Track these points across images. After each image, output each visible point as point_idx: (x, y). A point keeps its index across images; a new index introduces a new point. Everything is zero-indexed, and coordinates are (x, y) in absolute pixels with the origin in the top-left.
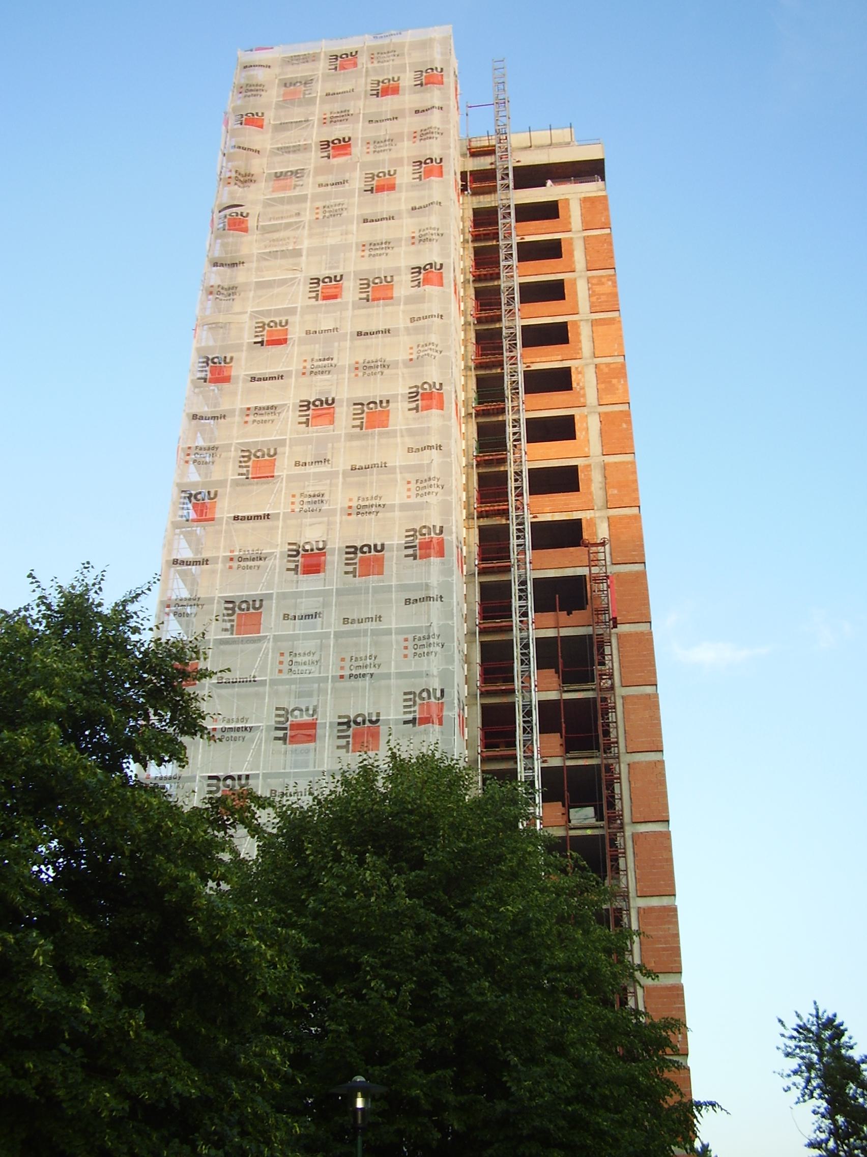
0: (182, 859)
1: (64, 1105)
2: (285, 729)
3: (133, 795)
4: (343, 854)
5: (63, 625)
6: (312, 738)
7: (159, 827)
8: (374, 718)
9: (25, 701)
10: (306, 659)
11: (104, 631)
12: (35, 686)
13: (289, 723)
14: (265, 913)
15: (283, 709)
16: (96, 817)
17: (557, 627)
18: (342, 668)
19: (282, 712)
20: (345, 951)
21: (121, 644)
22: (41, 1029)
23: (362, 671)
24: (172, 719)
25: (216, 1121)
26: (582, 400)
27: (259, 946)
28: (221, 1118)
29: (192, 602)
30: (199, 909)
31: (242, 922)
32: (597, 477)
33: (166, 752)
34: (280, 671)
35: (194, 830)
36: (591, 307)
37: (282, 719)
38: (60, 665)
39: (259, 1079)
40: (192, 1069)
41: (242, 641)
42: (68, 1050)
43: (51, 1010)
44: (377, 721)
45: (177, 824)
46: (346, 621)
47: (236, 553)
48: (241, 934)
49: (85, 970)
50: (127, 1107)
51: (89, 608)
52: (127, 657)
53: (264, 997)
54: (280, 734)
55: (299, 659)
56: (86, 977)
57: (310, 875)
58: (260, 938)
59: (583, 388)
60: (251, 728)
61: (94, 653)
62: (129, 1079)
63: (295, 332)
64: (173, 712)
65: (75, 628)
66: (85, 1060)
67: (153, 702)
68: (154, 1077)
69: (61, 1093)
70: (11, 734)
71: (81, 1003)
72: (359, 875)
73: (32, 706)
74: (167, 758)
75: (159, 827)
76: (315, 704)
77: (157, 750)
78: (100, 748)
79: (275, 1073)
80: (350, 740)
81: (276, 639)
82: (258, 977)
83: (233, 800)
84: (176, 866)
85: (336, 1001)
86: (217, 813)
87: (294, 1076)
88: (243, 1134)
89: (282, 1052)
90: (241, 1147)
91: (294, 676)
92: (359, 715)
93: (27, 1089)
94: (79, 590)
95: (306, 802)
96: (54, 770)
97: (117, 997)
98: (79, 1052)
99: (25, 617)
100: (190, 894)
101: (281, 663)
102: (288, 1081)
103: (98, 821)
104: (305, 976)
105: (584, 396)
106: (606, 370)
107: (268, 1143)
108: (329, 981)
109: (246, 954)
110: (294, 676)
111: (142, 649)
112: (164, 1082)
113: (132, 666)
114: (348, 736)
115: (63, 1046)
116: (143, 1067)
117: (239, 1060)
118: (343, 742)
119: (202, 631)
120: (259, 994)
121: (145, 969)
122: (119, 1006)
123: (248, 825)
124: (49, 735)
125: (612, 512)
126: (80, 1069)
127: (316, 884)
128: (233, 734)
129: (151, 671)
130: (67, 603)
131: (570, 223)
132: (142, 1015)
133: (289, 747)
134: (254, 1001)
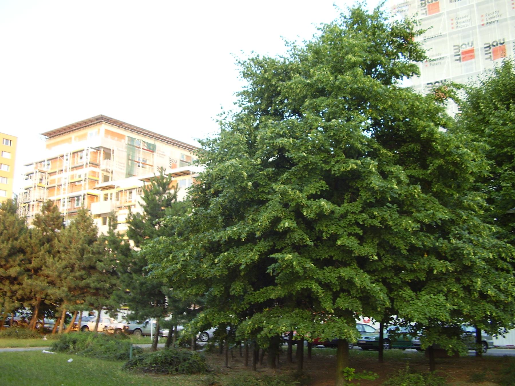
0: (426, 118)
1: (393, 228)
2: (459, 55)
3: (400, 93)
4: (499, 106)
5: (353, 24)
6: (472, 57)
7: (413, 105)
8: (502, 42)
9: (345, 61)
10: (464, 19)
11: (372, 22)
12: (347, 53)
13: (460, 52)
14: (467, 136)
15: (457, 46)
16: (385, 106)
19: (456, 47)
20: (505, 150)
21: (380, 27)
22: (378, 198)
23: (492, 20)
24: (410, 56)
25: (458, 229)
27: (467, 151)
28: (459, 227)
29: (405, 4)
30: (437, 139)
31: (457, 141)
33: (410, 71)
34: (453, 28)
35: (429, 104)
37: (457, 51)
38: (356, 42)
39: (474, 210)
40: (444, 208)
41: (432, 18)
42: (390, 205)
43: (381, 189)
44: (504, 43)
45: (421, 103)
48: (458, 147)
49: (392, 172)
50: (419, 226)
51: (363, 14)
52: (384, 32)
53: (472, 173)
54: (458, 58)
55: (460, 20)
56: (393, 174)
57: (484, 118)
58: (466, 148)
60: (443, 58)
61: (369, 33)
62: (418, 215)
64: (410, 52)
65: (358, 24)
66: (398, 209)
67: (400, 50)
68: (429, 212)
69: (390, 223)
70: (342, 76)
71: (393, 185)
72: (508, 115)
73: (348, 62)
74: (411, 75)
75: (413, 105)
76: (472, 40)
77: (406, 71)
78: (380, 76)
79: (481, 207)
80: (492, 54)
81: (448, 13)
82: (468, 165)
83: (445, 88)
84: (424, 121)
85: (504, 173)
86: (438, 95)
87: (489, 207)
88: (470, 233)
89: (482, 198)
90: (470, 239)
91: (459, 29)
92: (494, 42)
93: (376, 222)
94: (356, 8)
95: (478, 85)
96: (363, 89)
97: (407, 181)
98: (395, 206)
99: (336, 25)
100: (432, 133)
102: (487, 210)
103: (387, 107)
104: (490, 162)
107: (481, 236)
108: (500, 164)
109: (461, 156)
110: (459, 29)
111: (391, 27)
112: (434, 214)
113: (388, 36)
114: (490, 53)
115: (388, 204)
116: (423, 209)
117: (464, 202)
118: (488, 56)
119: (416, 12)
120: (470, 172)
121: (417, 168)
122: (408, 185)
123: (453, 98)
124: (358, 74)
126: (397, 213)
127: (488, 122)
129: (397, 36)
130: (353, 13)
132: (420, 187)
133: (463, 63)
134: (468, 176)
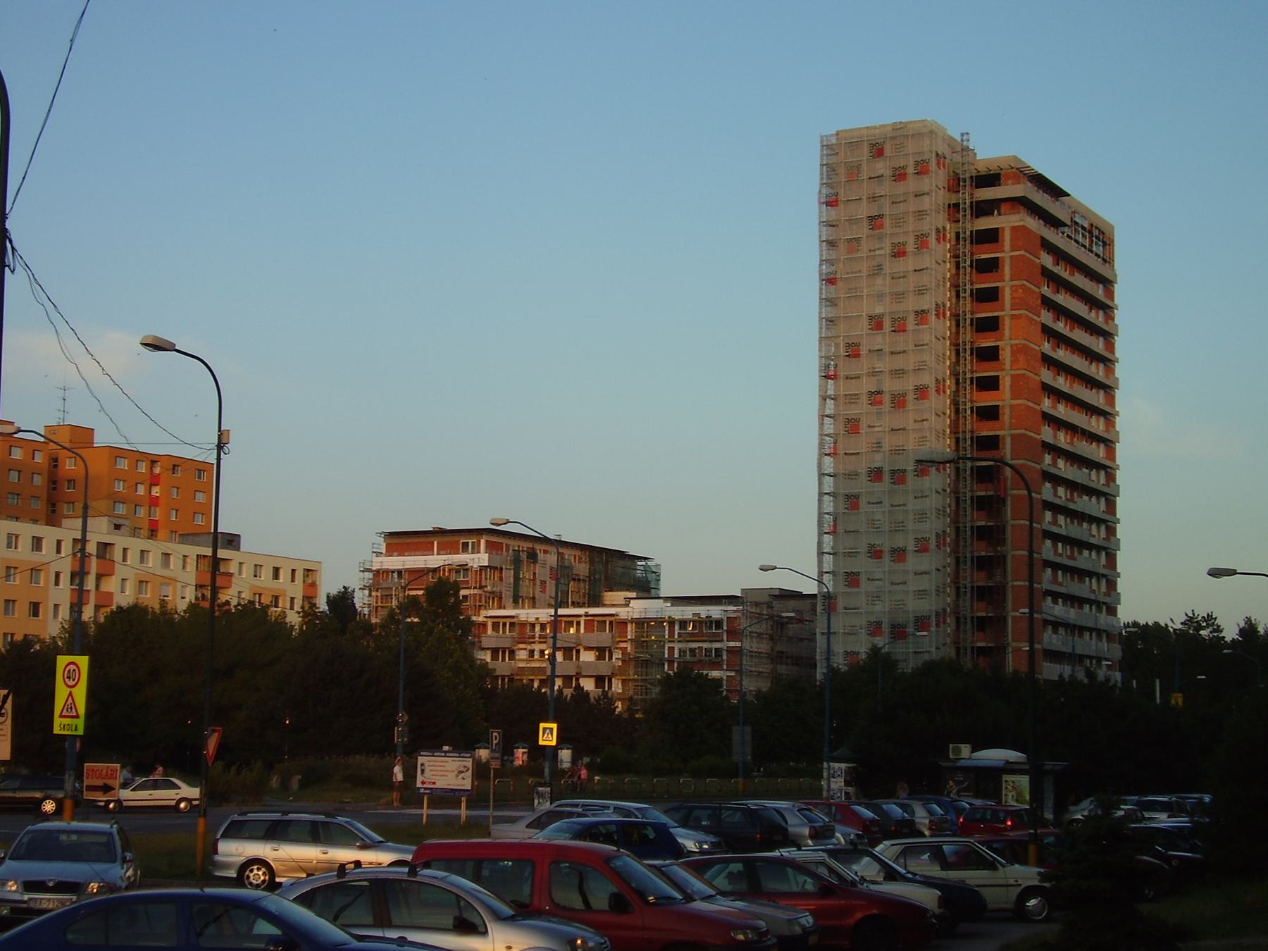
17: (986, 490)
18: (891, 527)
26: (1003, 366)
32: (1007, 411)
36: (1011, 306)
46: (892, 506)
47: (847, 472)
59: (1004, 360)
63: (864, 351)
101: (868, 524)
105: (1004, 364)
106: (1015, 348)
125: (1014, 432)
128: (852, 554)
131: (1004, 246)
